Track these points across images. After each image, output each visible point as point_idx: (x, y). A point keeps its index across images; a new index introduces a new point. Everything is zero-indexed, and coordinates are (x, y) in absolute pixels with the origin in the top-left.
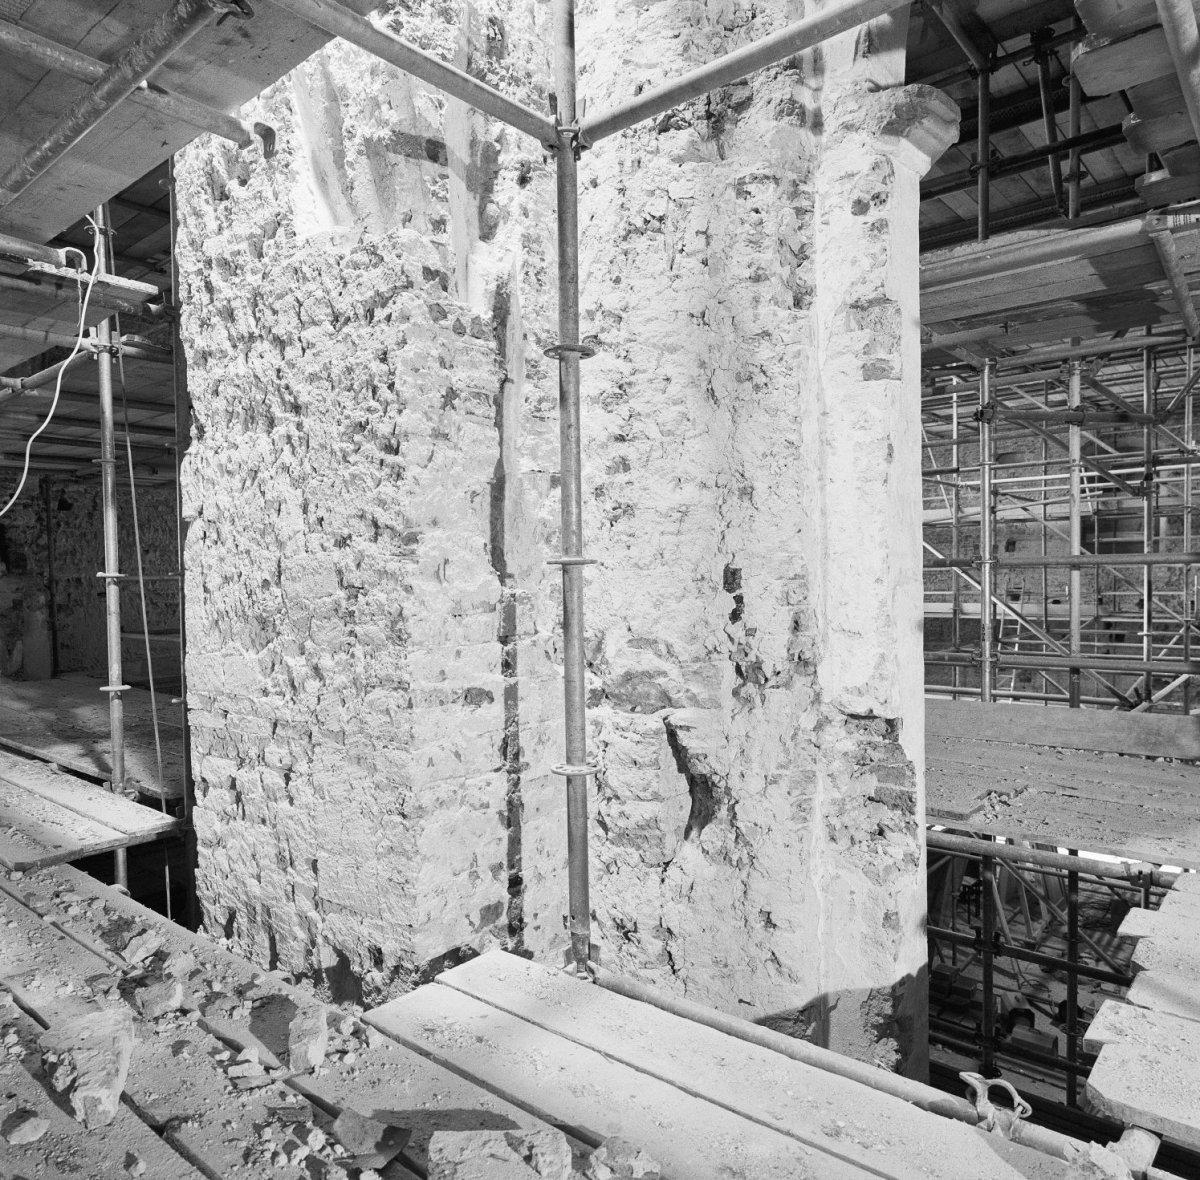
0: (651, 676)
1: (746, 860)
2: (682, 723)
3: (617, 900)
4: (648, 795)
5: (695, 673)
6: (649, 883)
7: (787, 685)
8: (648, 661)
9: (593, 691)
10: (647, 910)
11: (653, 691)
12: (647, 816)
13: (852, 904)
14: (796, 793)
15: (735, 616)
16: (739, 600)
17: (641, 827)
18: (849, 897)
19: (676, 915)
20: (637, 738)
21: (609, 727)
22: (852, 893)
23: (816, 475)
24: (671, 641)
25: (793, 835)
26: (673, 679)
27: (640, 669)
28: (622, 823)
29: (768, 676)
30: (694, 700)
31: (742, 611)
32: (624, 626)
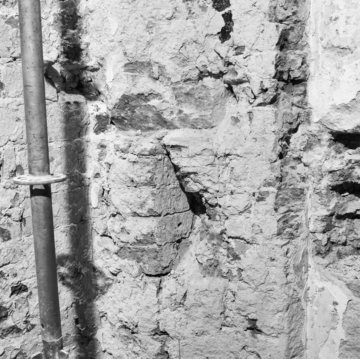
0: (146, 99)
1: (235, 272)
2: (174, 143)
3: (123, 305)
4: (144, 212)
5: (187, 94)
6: (147, 291)
7: (274, 101)
8: (144, 84)
9: (98, 117)
10: (147, 315)
11: (150, 114)
12: (145, 232)
13: (335, 313)
14: (282, 209)
15: (224, 34)
16: (228, 17)
17: (139, 242)
18: (332, 307)
19: (170, 320)
20: (134, 158)
21: (111, 148)
22: (335, 303)
23: (33, 145)
24: (163, 62)
25: (278, 249)
26: (166, 101)
27: (135, 92)
28: (124, 238)
29: (256, 93)
30: (184, 120)
31: (231, 30)
32: (120, 50)
